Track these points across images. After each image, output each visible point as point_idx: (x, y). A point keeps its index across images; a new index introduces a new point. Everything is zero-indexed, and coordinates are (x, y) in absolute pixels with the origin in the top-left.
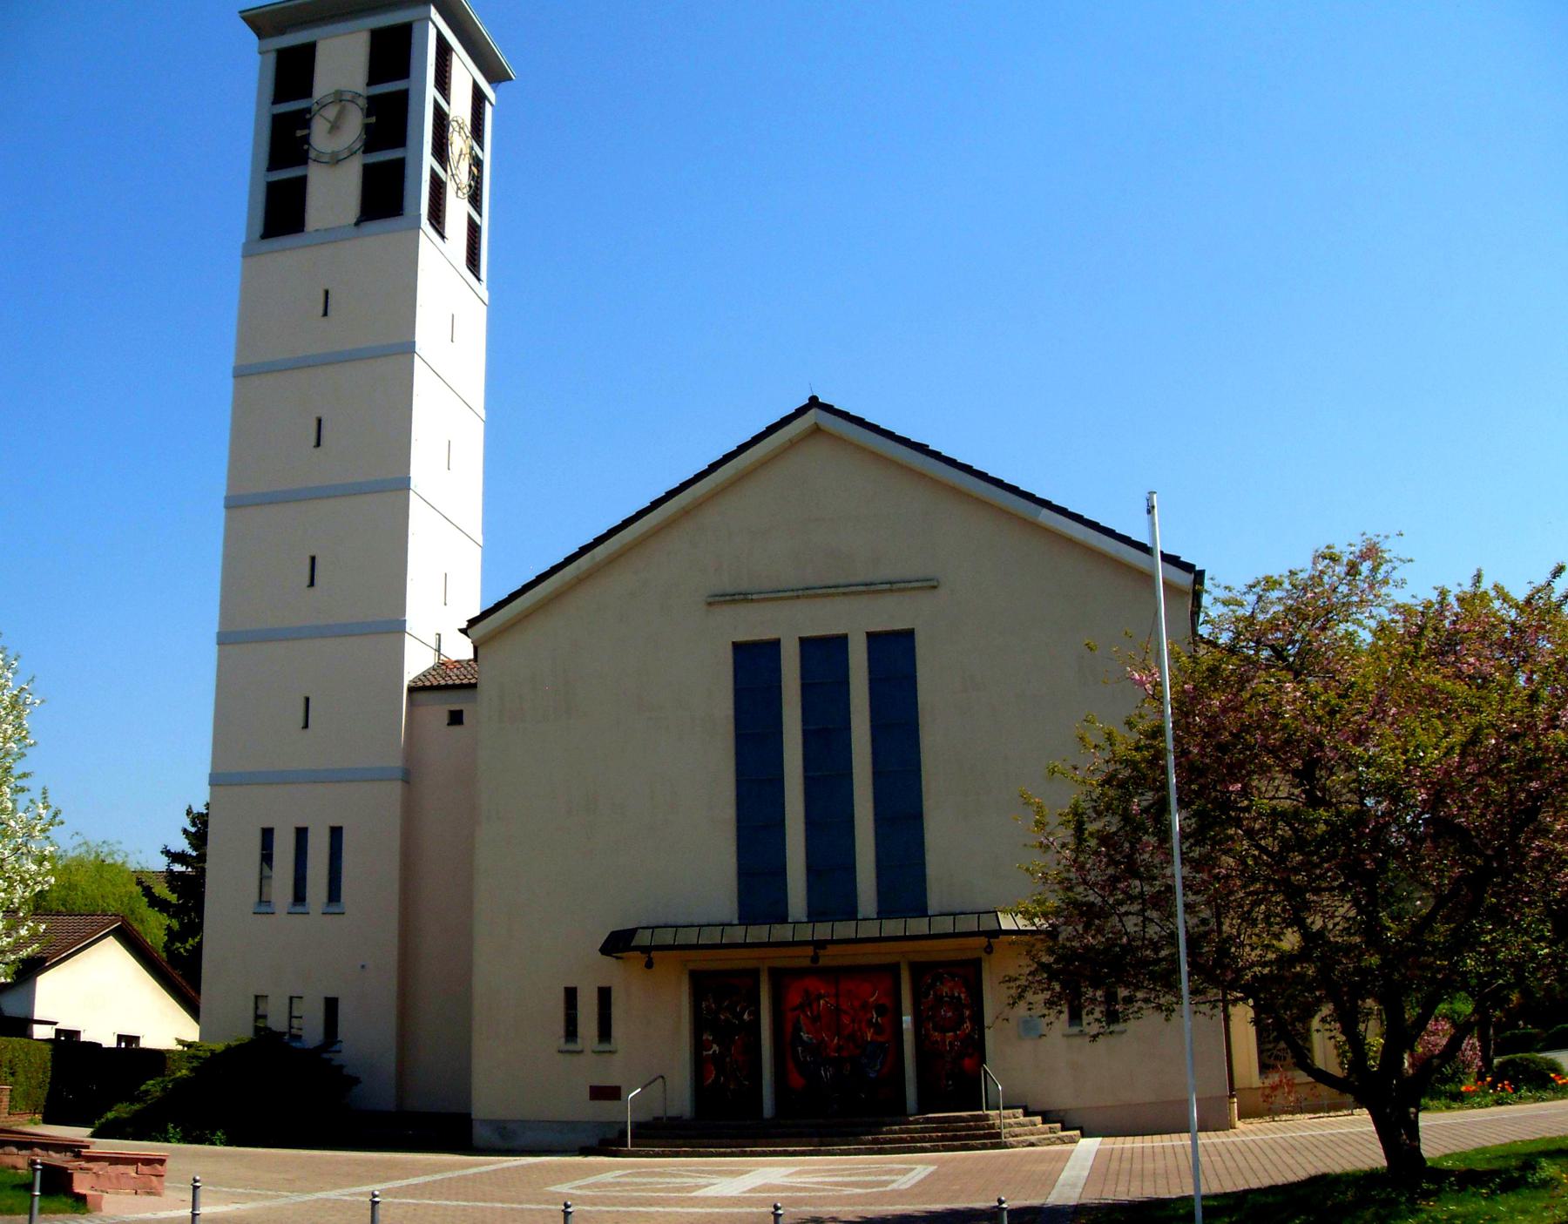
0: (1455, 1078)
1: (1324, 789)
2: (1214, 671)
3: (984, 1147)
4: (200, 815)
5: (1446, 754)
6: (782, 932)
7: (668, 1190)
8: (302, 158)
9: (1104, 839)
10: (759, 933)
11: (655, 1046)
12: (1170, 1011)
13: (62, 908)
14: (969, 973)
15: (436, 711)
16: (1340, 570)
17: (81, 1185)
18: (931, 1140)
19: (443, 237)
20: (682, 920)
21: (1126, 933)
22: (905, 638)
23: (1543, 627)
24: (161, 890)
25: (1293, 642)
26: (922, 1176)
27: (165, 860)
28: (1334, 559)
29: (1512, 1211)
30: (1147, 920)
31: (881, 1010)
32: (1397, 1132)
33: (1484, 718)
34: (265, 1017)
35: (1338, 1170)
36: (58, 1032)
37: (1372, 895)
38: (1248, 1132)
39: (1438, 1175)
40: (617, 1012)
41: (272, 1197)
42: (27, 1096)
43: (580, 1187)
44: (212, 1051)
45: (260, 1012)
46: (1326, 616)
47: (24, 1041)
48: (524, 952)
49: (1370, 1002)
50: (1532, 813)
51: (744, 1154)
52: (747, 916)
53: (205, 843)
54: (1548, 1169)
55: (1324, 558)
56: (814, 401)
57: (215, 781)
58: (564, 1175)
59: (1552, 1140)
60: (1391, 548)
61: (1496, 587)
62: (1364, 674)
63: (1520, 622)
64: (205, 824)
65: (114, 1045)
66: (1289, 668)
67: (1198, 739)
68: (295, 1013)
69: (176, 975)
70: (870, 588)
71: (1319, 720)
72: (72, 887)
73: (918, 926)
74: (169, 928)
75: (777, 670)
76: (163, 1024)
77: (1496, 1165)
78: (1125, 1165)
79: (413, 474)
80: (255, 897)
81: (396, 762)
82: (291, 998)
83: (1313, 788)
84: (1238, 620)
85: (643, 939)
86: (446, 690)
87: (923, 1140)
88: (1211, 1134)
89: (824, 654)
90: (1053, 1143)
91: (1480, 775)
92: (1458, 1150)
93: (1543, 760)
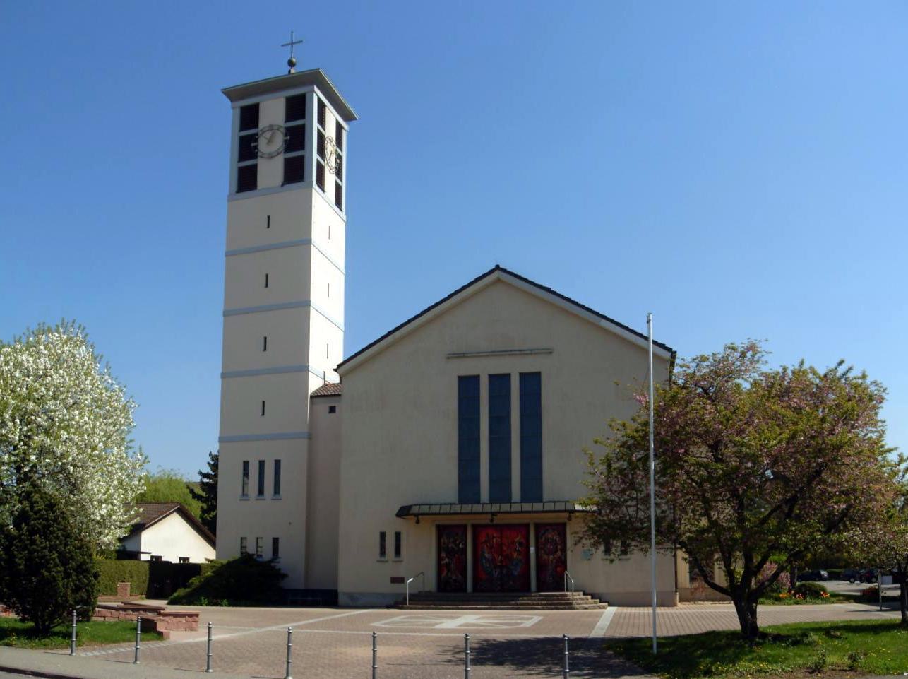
0: (777, 591)
1: (722, 455)
2: (674, 397)
3: (565, 609)
4: (216, 456)
5: (779, 443)
6: (477, 508)
7: (423, 625)
8: (255, 156)
9: (621, 471)
10: (467, 508)
11: (420, 560)
12: (646, 551)
13: (153, 500)
14: (561, 528)
15: (323, 406)
16: (737, 354)
17: (160, 627)
18: (541, 604)
19: (324, 191)
20: (432, 502)
21: (629, 515)
22: (536, 376)
23: (831, 388)
24: (198, 491)
25: (713, 387)
26: (536, 621)
27: (200, 477)
28: (734, 349)
29: (795, 655)
30: (638, 509)
31: (520, 544)
32: (747, 614)
33: (799, 427)
34: (245, 547)
35: (721, 629)
36: (152, 557)
37: (741, 505)
38: (683, 608)
39: (764, 635)
40: (403, 542)
41: (248, 630)
42: (138, 587)
43: (385, 624)
44: (222, 564)
45: (244, 545)
46: (729, 375)
47: (136, 562)
48: (363, 515)
49: (738, 553)
50: (818, 473)
51: (458, 609)
52: (463, 500)
53: (217, 468)
54: (814, 637)
55: (729, 348)
56: (497, 267)
57: (221, 440)
58: (379, 618)
59: (817, 623)
60: (762, 346)
61: (811, 368)
62: (744, 403)
63: (821, 385)
64: (217, 460)
65: (178, 562)
66: (710, 398)
67: (665, 428)
68: (260, 545)
69: (205, 529)
70: (522, 353)
71: (721, 423)
72: (156, 490)
73: (538, 507)
74: (202, 508)
75: (478, 389)
76: (199, 551)
77: (790, 633)
78: (627, 620)
79: (311, 299)
80: (241, 493)
81: (305, 429)
82: (257, 538)
83: (717, 454)
84: (687, 375)
85: (415, 510)
86: (327, 396)
87: (538, 604)
88: (666, 608)
89: (500, 382)
90: (595, 609)
91: (794, 453)
92: (775, 624)
93: (825, 449)
